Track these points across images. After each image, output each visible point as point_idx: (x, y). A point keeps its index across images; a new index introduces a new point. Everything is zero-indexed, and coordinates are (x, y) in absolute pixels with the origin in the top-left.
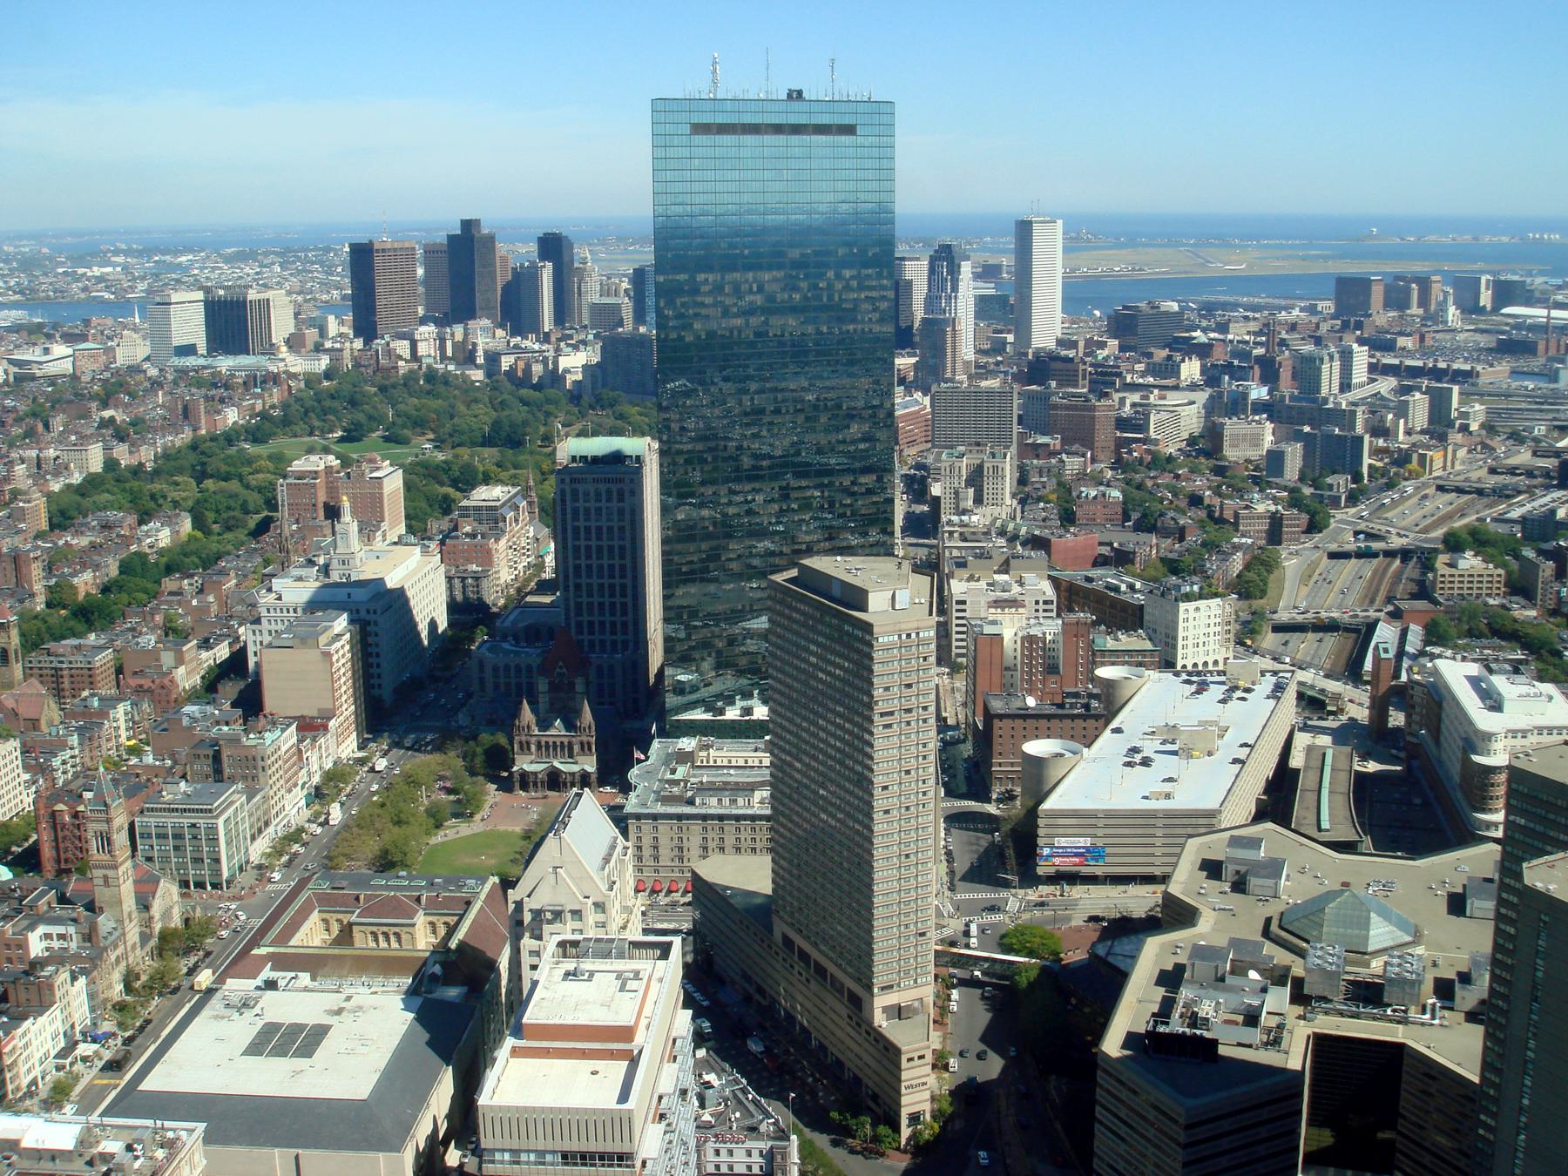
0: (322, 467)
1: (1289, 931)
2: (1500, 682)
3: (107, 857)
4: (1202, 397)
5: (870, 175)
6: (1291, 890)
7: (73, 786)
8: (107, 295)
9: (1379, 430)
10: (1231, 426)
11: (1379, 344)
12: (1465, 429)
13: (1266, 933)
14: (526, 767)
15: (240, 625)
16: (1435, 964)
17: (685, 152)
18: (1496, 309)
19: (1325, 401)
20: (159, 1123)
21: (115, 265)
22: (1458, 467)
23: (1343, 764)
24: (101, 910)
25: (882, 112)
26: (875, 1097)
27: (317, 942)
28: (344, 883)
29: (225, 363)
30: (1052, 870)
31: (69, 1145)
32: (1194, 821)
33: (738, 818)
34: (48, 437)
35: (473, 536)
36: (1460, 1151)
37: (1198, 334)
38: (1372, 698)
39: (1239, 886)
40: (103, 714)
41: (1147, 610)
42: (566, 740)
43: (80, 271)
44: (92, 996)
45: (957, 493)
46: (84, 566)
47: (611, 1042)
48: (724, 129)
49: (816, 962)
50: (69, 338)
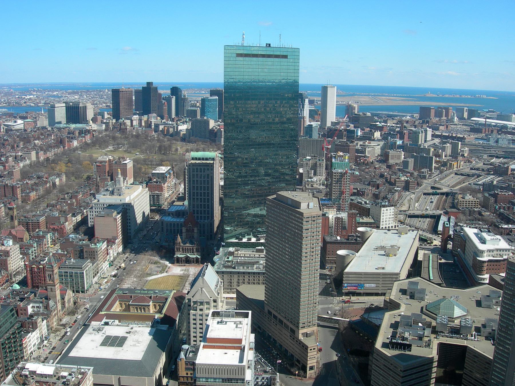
0: (107, 160)
1: (430, 311)
2: (485, 235)
3: (52, 282)
4: (382, 143)
5: (291, 71)
6: (429, 299)
7: (37, 259)
8: (32, 104)
9: (438, 155)
10: (391, 152)
11: (435, 128)
12: (463, 155)
13: (422, 311)
14: (178, 256)
15: (84, 209)
16: (474, 322)
17: (234, 62)
18: (469, 118)
19: (420, 145)
20: (79, 367)
21: (34, 95)
22: (461, 167)
23: (435, 259)
24: (50, 299)
25: (296, 51)
26: (298, 361)
27: (118, 310)
28: (127, 292)
29: (73, 126)
30: (347, 291)
31: (51, 373)
32: (392, 276)
33: (249, 273)
34: (18, 149)
35: (157, 182)
36: (483, 379)
37: (378, 123)
38: (442, 240)
39: (412, 297)
40: (44, 237)
41: (371, 210)
42: (191, 248)
43: (23, 97)
44: (48, 326)
45: (308, 172)
46: (33, 190)
47: (235, 343)
48: (247, 55)
50: (22, 118)
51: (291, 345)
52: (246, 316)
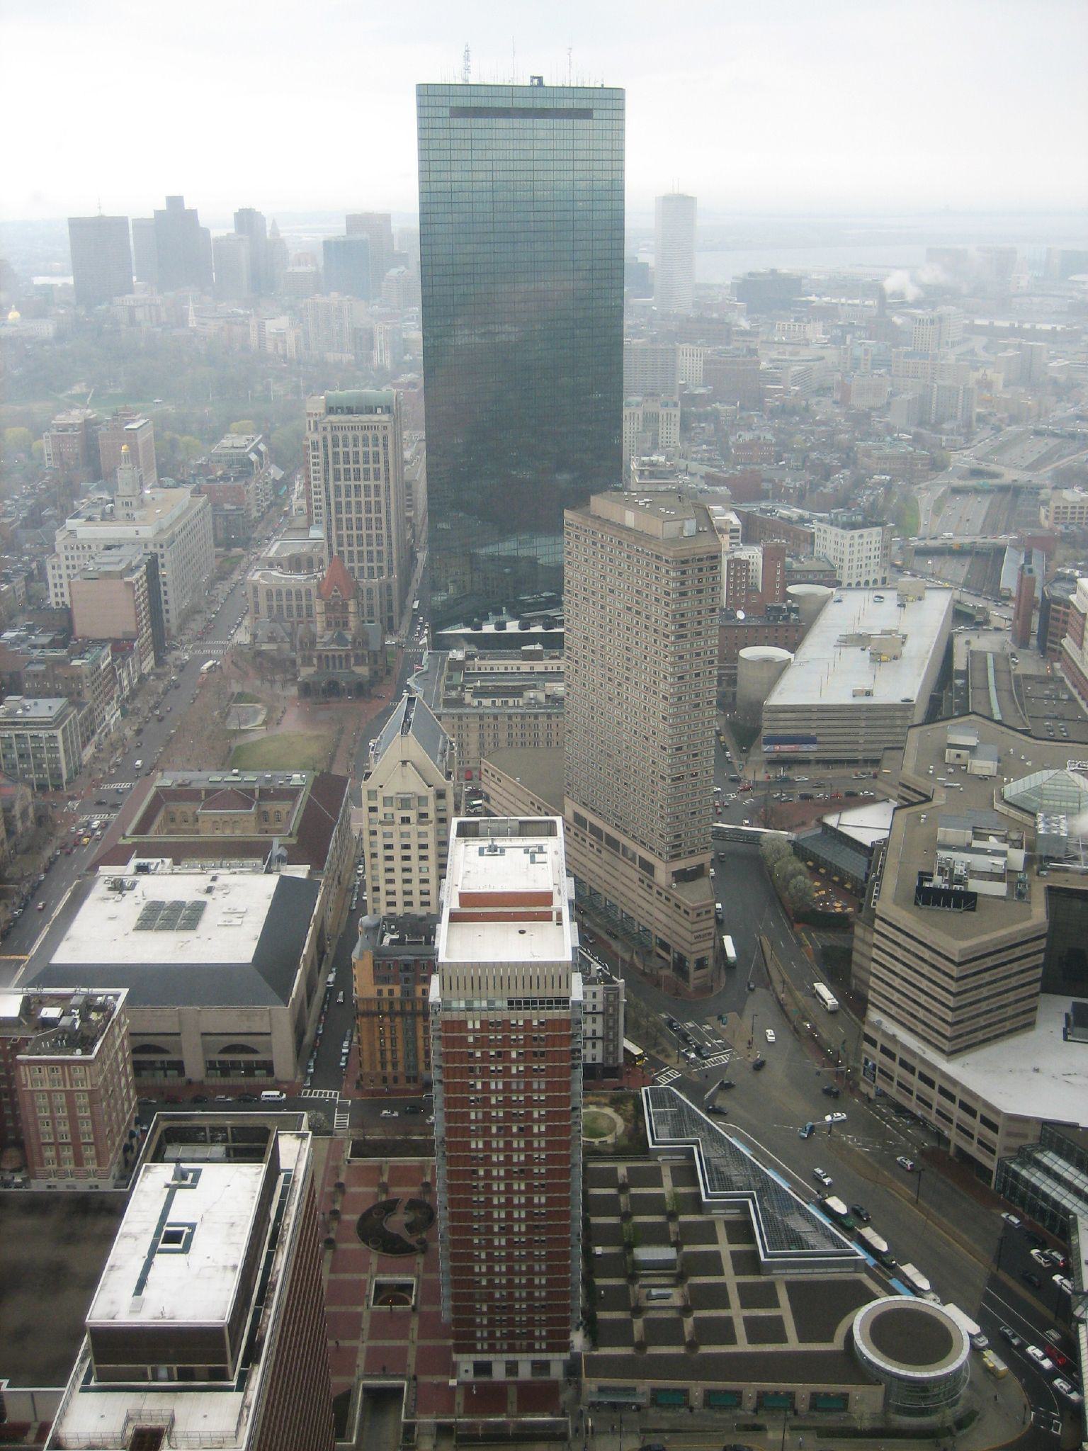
49: (607, 835)
51: (644, 904)
52: (550, 831)
